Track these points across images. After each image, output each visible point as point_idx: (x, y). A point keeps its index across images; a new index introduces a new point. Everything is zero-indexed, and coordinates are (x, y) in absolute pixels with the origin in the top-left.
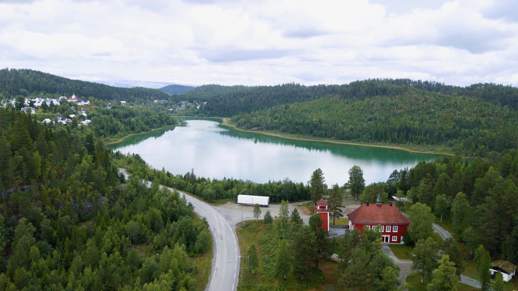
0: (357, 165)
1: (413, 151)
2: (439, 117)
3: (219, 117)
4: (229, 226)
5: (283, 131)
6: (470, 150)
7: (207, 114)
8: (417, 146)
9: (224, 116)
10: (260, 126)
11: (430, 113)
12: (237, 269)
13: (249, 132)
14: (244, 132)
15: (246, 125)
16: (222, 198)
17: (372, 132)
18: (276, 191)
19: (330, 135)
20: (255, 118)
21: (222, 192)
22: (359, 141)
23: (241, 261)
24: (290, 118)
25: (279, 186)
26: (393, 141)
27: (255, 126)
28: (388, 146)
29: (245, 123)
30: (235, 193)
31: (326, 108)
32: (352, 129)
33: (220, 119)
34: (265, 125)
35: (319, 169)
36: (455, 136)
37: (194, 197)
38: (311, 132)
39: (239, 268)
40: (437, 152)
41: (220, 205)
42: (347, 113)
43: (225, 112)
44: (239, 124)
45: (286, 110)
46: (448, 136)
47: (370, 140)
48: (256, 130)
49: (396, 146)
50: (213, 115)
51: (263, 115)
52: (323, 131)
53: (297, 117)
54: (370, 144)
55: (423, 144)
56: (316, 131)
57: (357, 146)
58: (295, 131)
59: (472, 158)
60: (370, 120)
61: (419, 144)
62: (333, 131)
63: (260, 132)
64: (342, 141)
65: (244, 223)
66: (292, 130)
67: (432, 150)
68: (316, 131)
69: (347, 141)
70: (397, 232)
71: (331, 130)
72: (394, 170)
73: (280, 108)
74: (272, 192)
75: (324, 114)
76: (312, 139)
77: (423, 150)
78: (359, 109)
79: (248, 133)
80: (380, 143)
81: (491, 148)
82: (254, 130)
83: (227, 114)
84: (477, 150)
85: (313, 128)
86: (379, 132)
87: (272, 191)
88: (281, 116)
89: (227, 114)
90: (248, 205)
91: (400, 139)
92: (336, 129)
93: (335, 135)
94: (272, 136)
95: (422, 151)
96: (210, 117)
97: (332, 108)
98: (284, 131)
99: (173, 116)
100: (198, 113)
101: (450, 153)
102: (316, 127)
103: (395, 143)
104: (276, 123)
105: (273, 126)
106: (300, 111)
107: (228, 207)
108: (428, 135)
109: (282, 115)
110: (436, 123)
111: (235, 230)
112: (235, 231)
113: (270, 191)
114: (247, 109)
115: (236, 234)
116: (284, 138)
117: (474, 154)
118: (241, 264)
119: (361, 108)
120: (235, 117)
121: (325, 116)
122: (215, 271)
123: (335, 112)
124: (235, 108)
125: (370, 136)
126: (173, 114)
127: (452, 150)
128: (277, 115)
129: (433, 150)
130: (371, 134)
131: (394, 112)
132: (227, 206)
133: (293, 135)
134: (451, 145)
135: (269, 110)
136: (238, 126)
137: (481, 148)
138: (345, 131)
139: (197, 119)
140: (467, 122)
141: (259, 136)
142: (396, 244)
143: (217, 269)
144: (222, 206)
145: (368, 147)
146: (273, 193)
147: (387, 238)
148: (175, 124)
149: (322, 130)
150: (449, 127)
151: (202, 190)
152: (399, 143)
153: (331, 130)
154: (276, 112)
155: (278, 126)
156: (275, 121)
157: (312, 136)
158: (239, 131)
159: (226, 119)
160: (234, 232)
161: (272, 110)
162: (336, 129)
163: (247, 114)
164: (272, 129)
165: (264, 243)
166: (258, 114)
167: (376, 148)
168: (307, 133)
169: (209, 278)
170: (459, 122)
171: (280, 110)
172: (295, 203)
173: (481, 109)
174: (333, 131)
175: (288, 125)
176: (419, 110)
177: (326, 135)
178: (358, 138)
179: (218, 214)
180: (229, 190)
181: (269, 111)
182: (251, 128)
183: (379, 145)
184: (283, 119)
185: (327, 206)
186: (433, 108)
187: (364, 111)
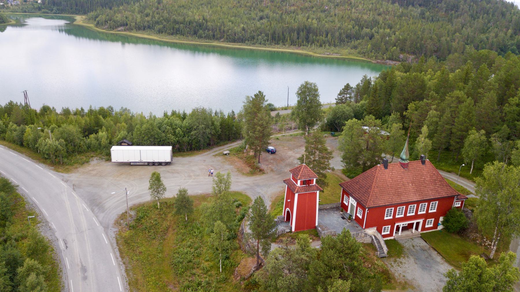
0: (311, 80)
1: (318, 55)
2: (335, 15)
3: (70, 14)
4: (101, 229)
5: (159, 32)
6: (380, 53)
7: (52, 10)
8: (320, 49)
9: (78, 12)
10: (127, 25)
11: (325, 11)
13: (113, 34)
14: (106, 34)
15: (108, 24)
16: (80, 152)
17: (268, 32)
18: (181, 132)
19: (219, 36)
20: (120, 15)
21: (77, 141)
22: (254, 44)
24: (166, 15)
25: (186, 123)
26: (293, 43)
27: (121, 25)
28: (288, 49)
29: (106, 21)
30: (104, 141)
31: (208, 3)
32: (243, 29)
33: (71, 17)
34: (134, 24)
35: (260, 92)
36: (357, 37)
37: (22, 153)
38: (195, 33)
40: (343, 55)
41: (77, 168)
42: (234, 10)
43: (77, 8)
44: (98, 23)
45: (159, 6)
46: (350, 37)
47: (266, 42)
48: (122, 31)
49: (297, 49)
50: (62, 11)
51: (130, 11)
52: (210, 32)
53: (175, 14)
54: (268, 47)
55: (325, 46)
56: (201, 31)
57: (251, 49)
58: (176, 32)
59: (383, 61)
60: (261, 18)
61: (321, 46)
62: (222, 31)
63: (128, 33)
64: (234, 43)
65: (133, 213)
66: (170, 30)
67: (337, 53)
68: (201, 31)
69: (240, 44)
70: (435, 211)
71: (220, 30)
72: (346, 85)
73: (150, 2)
74: (174, 134)
75: (207, 11)
76: (197, 41)
77: (328, 53)
78: (246, 6)
79: (111, 34)
80: (279, 46)
81: (402, 50)
82: (120, 31)
83: (81, 10)
84: (388, 53)
85: (197, 27)
86: (276, 32)
87: (175, 132)
88: (153, 13)
89: (81, 10)
90: (132, 164)
91: (300, 40)
92: (225, 29)
93: (225, 37)
94: (145, 38)
95: (328, 55)
96: (58, 14)
97: (215, 4)
98: (160, 32)
99: (4, 12)
100: (39, 9)
101: (357, 57)
102: (200, 25)
103: (295, 45)
104: (148, 22)
105: (145, 25)
106: (176, 6)
107: (94, 173)
108: (329, 35)
109: (155, 11)
110: (333, 22)
111: (114, 241)
112: (115, 245)
113: (171, 133)
114: (107, 4)
115: (118, 254)
116: (161, 41)
117: (385, 57)
119: (248, 4)
120: (92, 14)
121: (208, 13)
123: (219, 8)
124: (91, 2)
125: (266, 37)
126: (4, 10)
127: (359, 53)
128: (147, 11)
129: (338, 54)
130: (267, 35)
131: (286, 9)
132: (90, 169)
133: (173, 37)
134: (355, 47)
135: (137, 4)
136: (98, 24)
137: (392, 50)
138: (236, 31)
139: (40, 17)
140: (366, 21)
141: (128, 38)
142: (430, 231)
144: (81, 169)
145: (265, 51)
146: (177, 136)
147: (418, 224)
148: (5, 23)
149: (209, 30)
150: (348, 26)
151: (35, 140)
152: (300, 45)
153: (220, 30)
154: (146, 7)
155: (151, 26)
156: (146, 18)
157: (197, 38)
158: (99, 32)
159: (80, 17)
160: (114, 249)
161: (140, 5)
162: (225, 29)
163: (108, 10)
164: (144, 29)
165: (186, 269)
166: (123, 9)
167: (274, 52)
168: (190, 34)
170: (357, 22)
171: (150, 5)
172: (215, 149)
173: (376, 7)
174: (222, 31)
175: (165, 23)
176: (313, 8)
177: (214, 36)
178: (252, 39)
179: (74, 194)
180: (92, 136)
181: (137, 7)
182: (116, 28)
183: (278, 48)
184: (157, 16)
185: (315, 179)
186: (327, 5)
187: (252, 8)
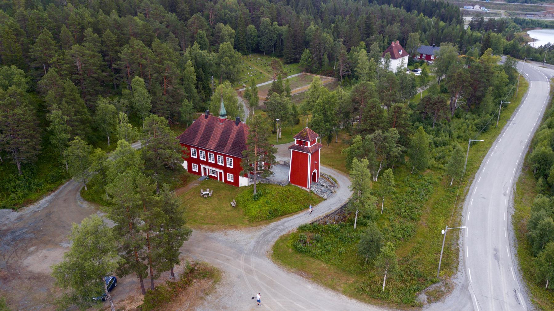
12: (474, 187)
23: (465, 196)
39: (471, 188)
112: (461, 263)
115: (461, 254)
118: (467, 192)
122: (507, 192)
143: (505, 195)
169: (515, 187)
